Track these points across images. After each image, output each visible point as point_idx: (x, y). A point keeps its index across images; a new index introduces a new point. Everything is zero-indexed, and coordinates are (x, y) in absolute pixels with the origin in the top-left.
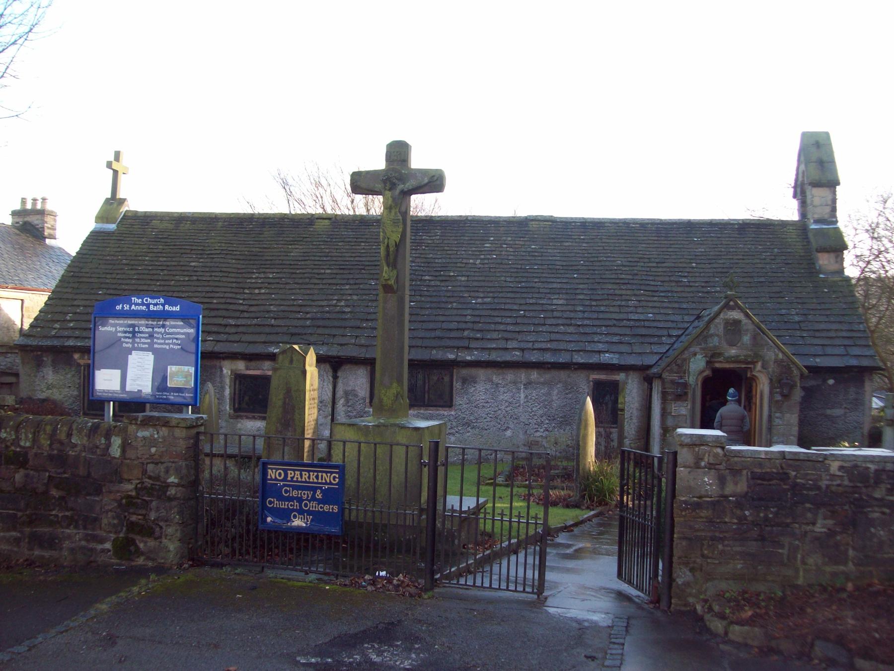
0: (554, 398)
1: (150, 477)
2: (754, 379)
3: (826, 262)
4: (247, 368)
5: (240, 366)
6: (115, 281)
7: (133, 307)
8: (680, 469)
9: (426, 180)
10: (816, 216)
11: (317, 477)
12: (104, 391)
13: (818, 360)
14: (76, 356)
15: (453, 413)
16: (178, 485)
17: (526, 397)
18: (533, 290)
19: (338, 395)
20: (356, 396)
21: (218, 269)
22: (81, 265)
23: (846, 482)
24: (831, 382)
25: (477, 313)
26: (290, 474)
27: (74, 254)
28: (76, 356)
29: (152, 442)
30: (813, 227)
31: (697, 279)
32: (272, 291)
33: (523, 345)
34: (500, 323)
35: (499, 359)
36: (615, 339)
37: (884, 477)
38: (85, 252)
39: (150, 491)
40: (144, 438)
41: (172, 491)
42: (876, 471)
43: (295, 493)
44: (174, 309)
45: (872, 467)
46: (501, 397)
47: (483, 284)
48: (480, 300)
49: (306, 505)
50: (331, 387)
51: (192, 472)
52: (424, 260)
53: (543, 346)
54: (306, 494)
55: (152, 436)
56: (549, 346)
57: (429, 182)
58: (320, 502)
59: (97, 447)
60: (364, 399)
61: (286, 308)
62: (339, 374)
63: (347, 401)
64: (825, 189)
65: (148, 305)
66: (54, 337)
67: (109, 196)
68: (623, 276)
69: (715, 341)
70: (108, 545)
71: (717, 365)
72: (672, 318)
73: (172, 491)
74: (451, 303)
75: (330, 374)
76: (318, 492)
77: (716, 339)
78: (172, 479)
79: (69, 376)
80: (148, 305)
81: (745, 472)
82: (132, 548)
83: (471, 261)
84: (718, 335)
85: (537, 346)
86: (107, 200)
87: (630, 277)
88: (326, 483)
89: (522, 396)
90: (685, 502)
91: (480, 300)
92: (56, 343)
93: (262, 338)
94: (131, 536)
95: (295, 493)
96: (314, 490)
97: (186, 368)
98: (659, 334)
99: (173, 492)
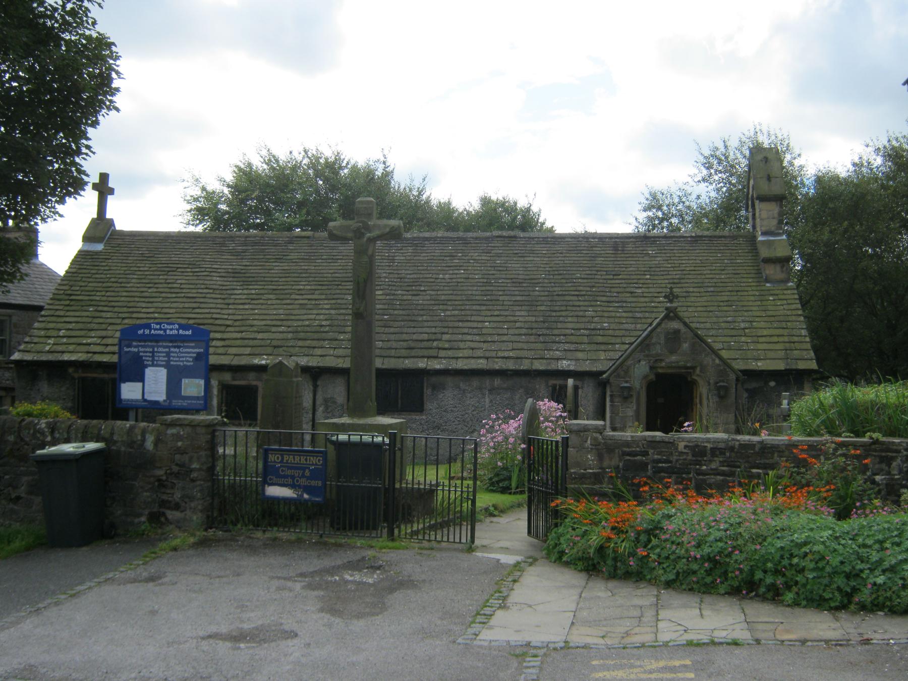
0: (517, 402)
1: (177, 465)
2: (694, 383)
3: (772, 272)
4: (234, 379)
5: (227, 377)
6: (104, 298)
7: (153, 332)
8: (570, 449)
9: (388, 230)
10: (764, 229)
11: (306, 460)
12: (128, 400)
13: (759, 364)
14: (71, 370)
15: (424, 417)
16: (200, 470)
17: (491, 401)
18: (498, 303)
19: (318, 403)
20: (335, 402)
21: (203, 286)
22: (71, 283)
23: (690, 457)
24: (772, 384)
25: (446, 324)
26: (286, 458)
27: (62, 273)
28: (71, 370)
29: (178, 437)
30: (760, 238)
31: (651, 290)
32: (254, 307)
33: (488, 354)
34: (467, 334)
35: (466, 367)
36: (572, 347)
37: (718, 453)
38: (74, 270)
39: (177, 475)
40: (173, 435)
41: (194, 475)
42: (711, 448)
43: (289, 472)
44: (187, 333)
45: (709, 446)
46: (468, 402)
47: (450, 297)
48: (448, 313)
49: (297, 481)
50: (311, 395)
51: (210, 460)
52: (396, 276)
53: (506, 354)
54: (297, 473)
55: (179, 433)
56: (511, 354)
57: (390, 232)
58: (308, 478)
59: (135, 442)
60: (342, 406)
61: (269, 322)
62: (319, 383)
63: (327, 407)
64: (774, 203)
65: (165, 330)
66: (49, 352)
67: (96, 216)
68: (581, 288)
69: (658, 349)
70: (143, 519)
71: (660, 371)
72: (626, 326)
73: (194, 475)
74: (422, 315)
75: (311, 383)
76: (307, 471)
77: (658, 347)
78: (195, 466)
79: (63, 389)
80: (165, 330)
81: (617, 451)
82: (163, 519)
83: (441, 276)
84: (660, 344)
85: (500, 354)
86: (93, 220)
87: (588, 289)
88: (313, 464)
89: (487, 400)
90: (574, 473)
91: (448, 313)
92: (51, 357)
93: (248, 351)
94: (162, 510)
95: (289, 472)
96: (304, 469)
97: (197, 381)
98: (613, 341)
99: (195, 475)
